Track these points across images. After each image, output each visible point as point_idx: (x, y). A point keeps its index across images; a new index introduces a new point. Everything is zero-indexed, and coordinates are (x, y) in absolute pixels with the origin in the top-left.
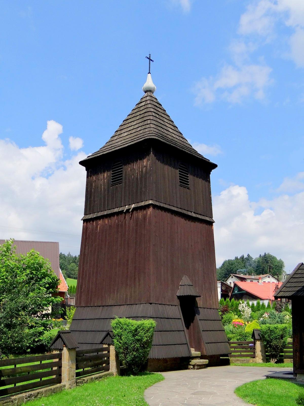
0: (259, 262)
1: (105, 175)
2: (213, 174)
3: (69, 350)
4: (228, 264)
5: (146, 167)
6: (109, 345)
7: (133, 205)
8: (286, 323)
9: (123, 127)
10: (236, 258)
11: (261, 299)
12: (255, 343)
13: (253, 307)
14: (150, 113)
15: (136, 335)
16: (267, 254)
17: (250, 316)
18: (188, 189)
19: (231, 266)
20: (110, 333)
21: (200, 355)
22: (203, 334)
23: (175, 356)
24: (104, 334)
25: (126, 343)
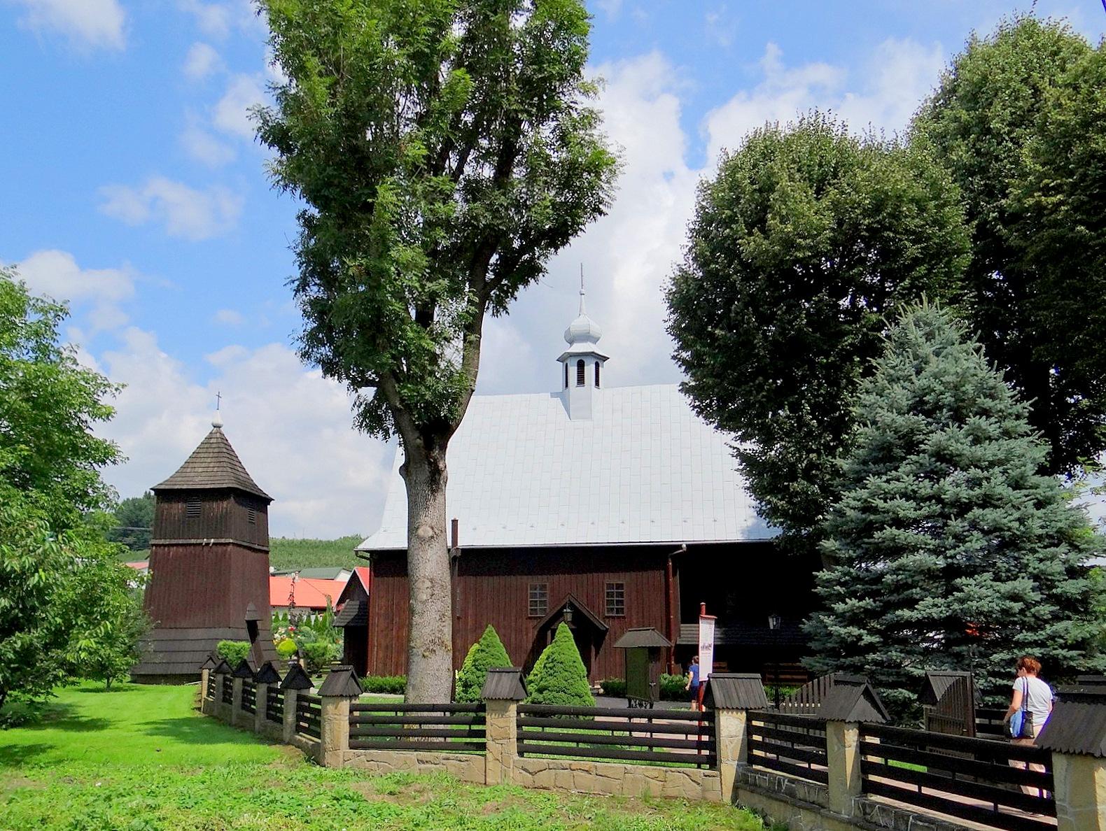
4: (132, 508)
5: (227, 509)
9: (194, 460)
19: (138, 512)
22: (264, 653)
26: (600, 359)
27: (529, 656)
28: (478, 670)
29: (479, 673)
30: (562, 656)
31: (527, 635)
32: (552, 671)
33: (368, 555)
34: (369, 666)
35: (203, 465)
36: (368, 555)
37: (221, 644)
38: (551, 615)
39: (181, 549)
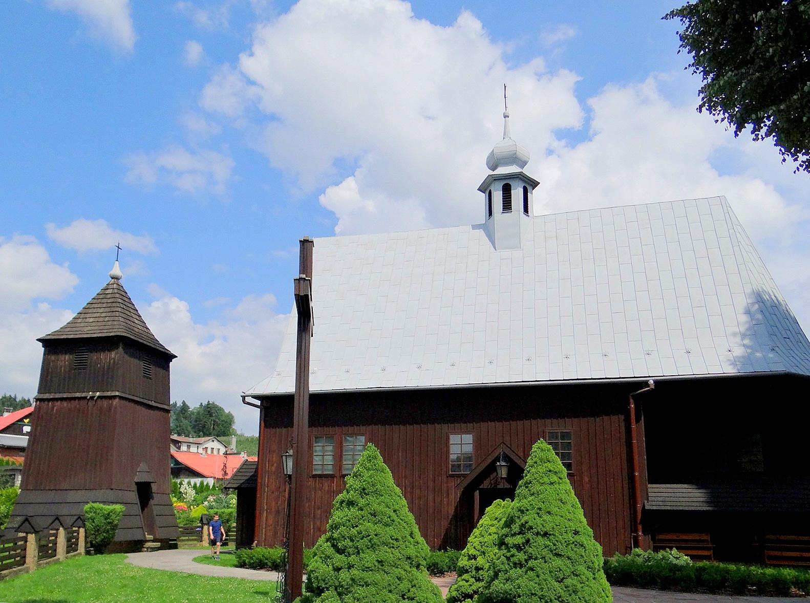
0: (198, 413)
1: (67, 357)
2: (173, 364)
3: (65, 529)
5: (114, 359)
6: (79, 528)
7: (98, 393)
8: (232, 508)
9: (87, 311)
11: (203, 476)
12: (202, 528)
13: (195, 487)
15: (108, 518)
16: (210, 402)
17: (193, 499)
18: (150, 379)
20: (81, 517)
21: (152, 539)
24: (53, 518)
25: (98, 525)
26: (530, 184)
27: (450, 523)
28: (340, 551)
29: (339, 559)
31: (448, 497)
32: (521, 556)
34: (256, 534)
35: (95, 315)
37: (87, 507)
38: (475, 475)
39: (65, 404)
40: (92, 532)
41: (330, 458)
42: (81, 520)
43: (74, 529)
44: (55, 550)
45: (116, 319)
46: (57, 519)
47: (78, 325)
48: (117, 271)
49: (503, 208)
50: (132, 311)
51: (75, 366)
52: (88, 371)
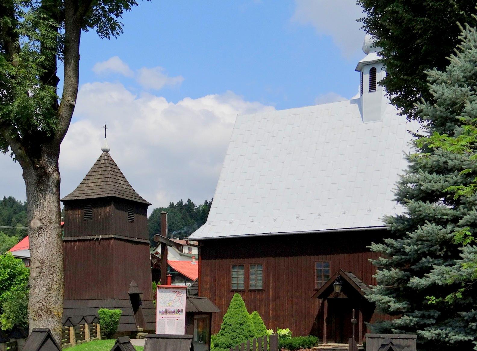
3: (88, 324)
5: (109, 213)
6: (96, 323)
7: (101, 236)
9: (89, 178)
10: (172, 205)
14: (108, 172)
15: (112, 318)
20: (97, 317)
22: (145, 317)
23: (128, 330)
30: (232, 320)
33: (197, 243)
35: (95, 181)
36: (197, 243)
37: (99, 311)
39: (81, 244)
40: (104, 326)
41: (242, 279)
42: (97, 319)
43: (94, 324)
44: (84, 336)
45: (108, 183)
46: (83, 318)
47: (84, 189)
48: (106, 146)
49: (370, 88)
50: (118, 175)
51: (85, 218)
52: (93, 220)
